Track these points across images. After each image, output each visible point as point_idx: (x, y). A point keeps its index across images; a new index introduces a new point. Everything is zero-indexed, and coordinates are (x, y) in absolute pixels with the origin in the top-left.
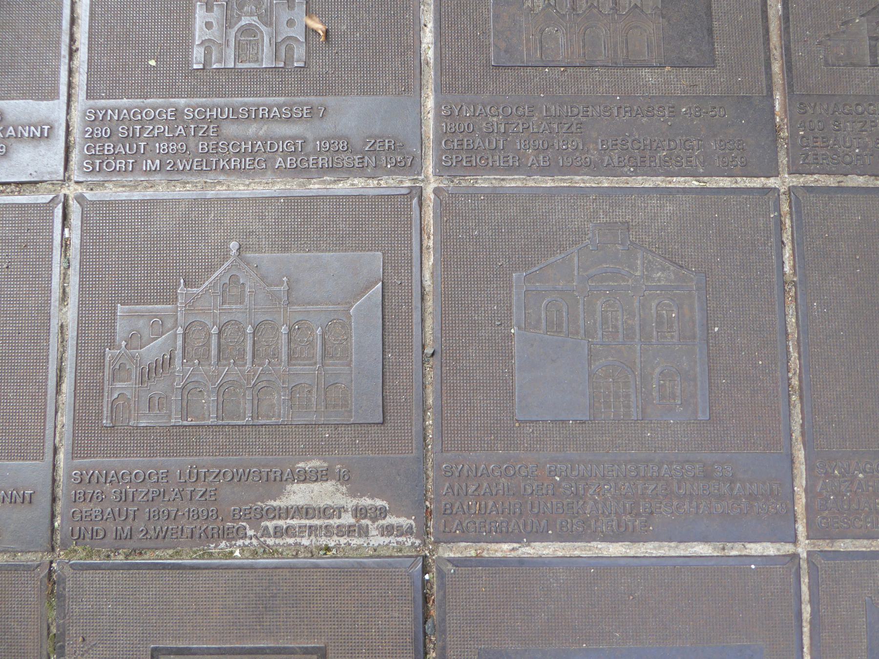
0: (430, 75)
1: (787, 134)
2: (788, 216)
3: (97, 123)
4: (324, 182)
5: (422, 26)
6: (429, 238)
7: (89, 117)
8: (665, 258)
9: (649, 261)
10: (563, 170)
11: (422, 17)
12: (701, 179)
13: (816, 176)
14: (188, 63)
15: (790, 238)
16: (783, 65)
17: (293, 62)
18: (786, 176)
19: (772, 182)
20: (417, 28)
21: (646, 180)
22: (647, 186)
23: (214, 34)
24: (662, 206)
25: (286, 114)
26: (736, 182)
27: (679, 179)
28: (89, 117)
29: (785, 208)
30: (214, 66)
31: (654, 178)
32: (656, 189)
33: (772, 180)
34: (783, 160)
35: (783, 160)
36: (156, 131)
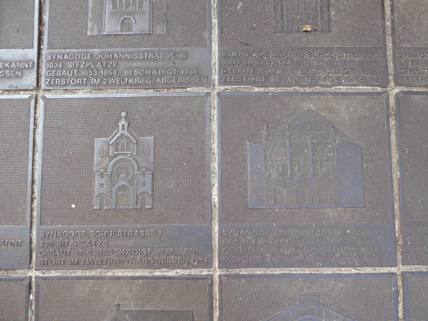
0: (216, 213)
1: (401, 243)
2: (401, 287)
3: (46, 238)
4: (162, 271)
5: (212, 185)
6: (216, 301)
7: (49, 58)
8: (338, 312)
9: (330, 314)
10: (285, 265)
11: (212, 181)
12: (357, 268)
13: (416, 266)
14: (92, 206)
15: (402, 299)
16: (400, 205)
17: (145, 206)
18: (401, 265)
19: (393, 270)
20: (210, 187)
21: (328, 269)
22: (329, 273)
23: (105, 190)
24: (336, 284)
25: (141, 57)
26: (375, 270)
27: (345, 268)
28: (49, 58)
29: (400, 283)
30: (105, 208)
31: (332, 268)
32: (333, 275)
33: (393, 268)
34: (399, 257)
35: (399, 257)
36: (87, 65)
